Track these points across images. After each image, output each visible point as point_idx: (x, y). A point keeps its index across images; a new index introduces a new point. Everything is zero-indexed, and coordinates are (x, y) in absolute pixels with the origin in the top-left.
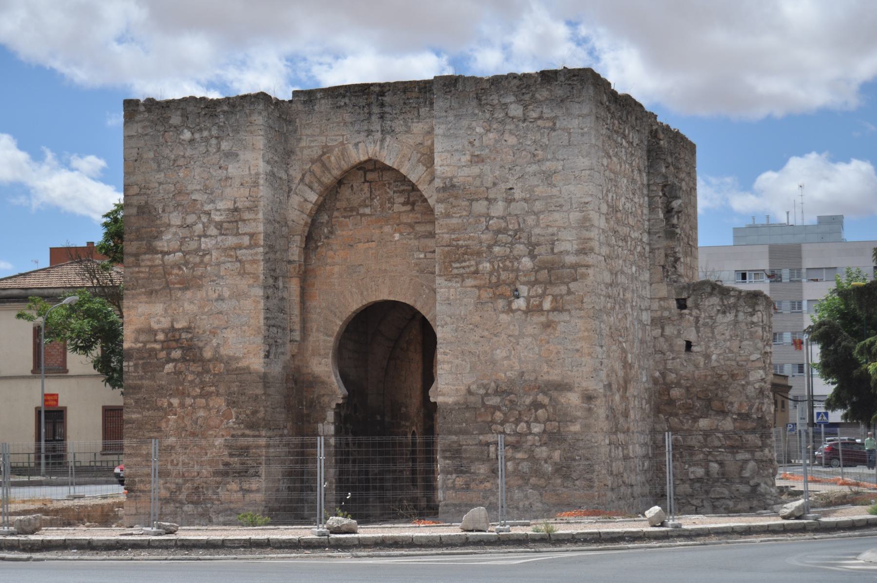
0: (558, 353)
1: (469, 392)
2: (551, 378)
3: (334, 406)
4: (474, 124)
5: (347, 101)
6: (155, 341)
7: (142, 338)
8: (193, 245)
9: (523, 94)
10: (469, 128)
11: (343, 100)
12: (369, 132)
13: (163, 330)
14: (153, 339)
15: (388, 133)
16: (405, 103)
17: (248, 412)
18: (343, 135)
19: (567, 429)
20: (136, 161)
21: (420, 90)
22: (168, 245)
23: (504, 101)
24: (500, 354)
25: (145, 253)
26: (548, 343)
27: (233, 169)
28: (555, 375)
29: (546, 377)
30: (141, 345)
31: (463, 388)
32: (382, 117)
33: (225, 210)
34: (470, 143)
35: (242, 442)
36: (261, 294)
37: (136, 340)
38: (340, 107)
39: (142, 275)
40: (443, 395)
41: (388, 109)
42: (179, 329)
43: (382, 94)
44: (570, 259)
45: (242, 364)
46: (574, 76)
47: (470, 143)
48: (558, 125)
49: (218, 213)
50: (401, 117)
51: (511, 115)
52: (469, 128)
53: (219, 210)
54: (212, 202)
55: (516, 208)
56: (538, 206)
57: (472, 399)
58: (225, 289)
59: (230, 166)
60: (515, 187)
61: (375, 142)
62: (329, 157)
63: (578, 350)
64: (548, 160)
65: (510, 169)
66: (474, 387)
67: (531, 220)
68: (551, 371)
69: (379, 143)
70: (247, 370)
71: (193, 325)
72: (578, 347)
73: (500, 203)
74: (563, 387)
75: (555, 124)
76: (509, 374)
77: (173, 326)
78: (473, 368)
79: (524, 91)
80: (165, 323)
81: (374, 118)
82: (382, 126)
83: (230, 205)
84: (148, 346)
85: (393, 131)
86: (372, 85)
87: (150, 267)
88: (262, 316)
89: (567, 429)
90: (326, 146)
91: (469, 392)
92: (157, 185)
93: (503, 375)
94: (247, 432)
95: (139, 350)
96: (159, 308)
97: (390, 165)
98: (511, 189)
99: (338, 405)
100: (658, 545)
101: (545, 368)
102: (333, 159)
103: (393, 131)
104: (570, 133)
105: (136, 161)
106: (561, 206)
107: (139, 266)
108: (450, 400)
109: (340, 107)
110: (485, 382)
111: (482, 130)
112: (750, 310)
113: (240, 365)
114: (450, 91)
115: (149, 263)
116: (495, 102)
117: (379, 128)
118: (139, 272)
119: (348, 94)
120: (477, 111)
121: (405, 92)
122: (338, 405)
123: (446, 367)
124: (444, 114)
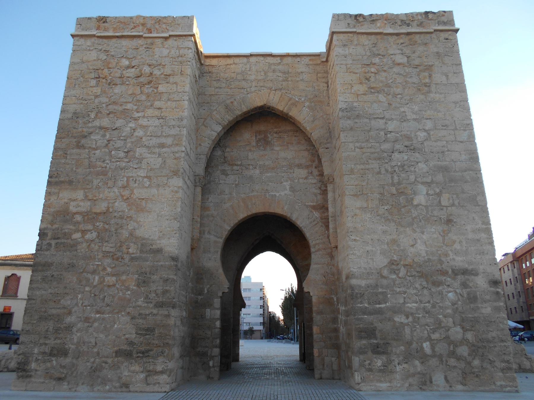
3: (220, 294)
96: (80, 194)
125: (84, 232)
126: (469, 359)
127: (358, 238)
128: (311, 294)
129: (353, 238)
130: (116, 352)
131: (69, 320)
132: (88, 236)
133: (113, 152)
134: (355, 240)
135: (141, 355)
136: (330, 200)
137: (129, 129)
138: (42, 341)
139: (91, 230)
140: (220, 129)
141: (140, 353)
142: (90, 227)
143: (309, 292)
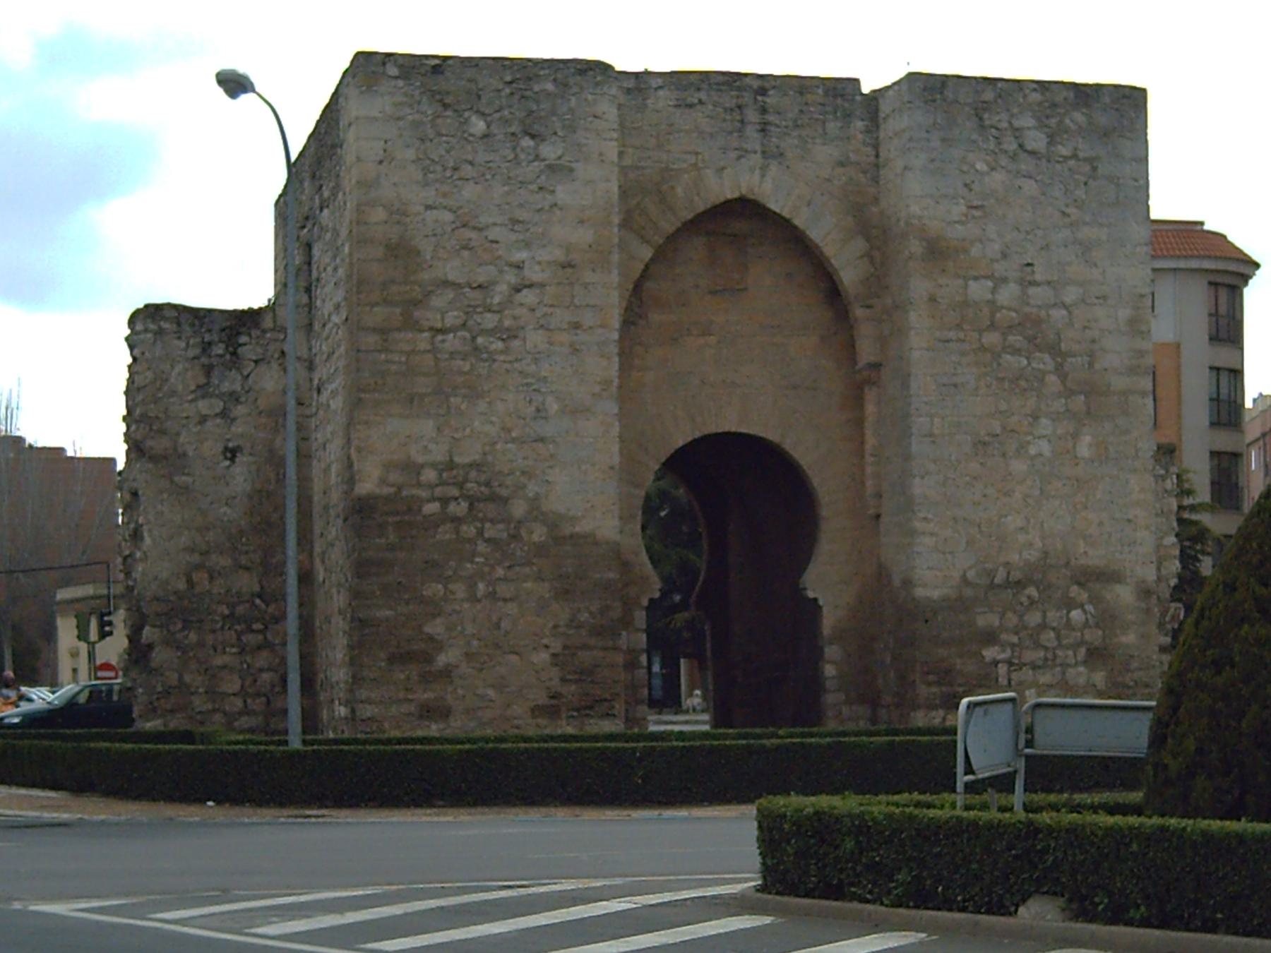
0: (1101, 524)
1: (965, 580)
2: (1090, 563)
3: (645, 603)
4: (971, 156)
5: (703, 95)
6: (419, 485)
7: (394, 477)
8: (490, 320)
9: (1047, 117)
10: (964, 160)
11: (696, 95)
12: (743, 153)
13: (433, 465)
14: (414, 482)
15: (773, 157)
16: (801, 111)
17: (593, 609)
18: (697, 154)
19: (1116, 640)
20: (381, 162)
21: (826, 93)
22: (443, 319)
23: (1016, 123)
24: (1014, 521)
25: (399, 330)
26: (1086, 508)
27: (563, 193)
28: (1095, 558)
29: (1082, 561)
30: (392, 490)
31: (956, 575)
32: (763, 130)
33: (549, 263)
34: (966, 185)
35: (585, 657)
36: (616, 410)
37: (383, 481)
38: (691, 106)
39: (394, 368)
40: (925, 585)
41: (771, 118)
42: (464, 466)
43: (763, 91)
44: (1119, 383)
45: (583, 527)
46: (1124, 97)
47: (966, 185)
48: (1100, 171)
49: (537, 268)
50: (795, 133)
51: (1029, 148)
52: (964, 160)
53: (539, 263)
54: (528, 245)
55: (1039, 294)
56: (1071, 294)
57: (968, 592)
58: (550, 399)
59: (559, 188)
60: (1035, 262)
61: (752, 170)
62: (673, 188)
63: (1129, 521)
64: (1085, 223)
65: (1028, 233)
66: (971, 575)
67: (1058, 314)
68: (1091, 553)
69: (757, 172)
70: (590, 539)
71: (490, 458)
72: (1131, 517)
73: (1012, 285)
74: (1109, 576)
75: (1094, 169)
76: (1025, 555)
77: (451, 461)
78: (970, 543)
79: (1048, 111)
80: (438, 453)
81: (751, 132)
82: (763, 145)
83: (559, 255)
84: (404, 493)
85: (782, 154)
86: (746, 75)
87: (408, 354)
88: (616, 448)
89: (1116, 640)
90: (667, 169)
91: (965, 580)
92: (421, 209)
93: (1017, 557)
94: (592, 641)
95: (388, 499)
96: (427, 427)
97: (778, 211)
98: (1029, 265)
99: (651, 600)
100: (355, 820)
101: (1082, 547)
102: (679, 190)
103: (782, 154)
104: (1118, 185)
105: (381, 162)
106: (1104, 298)
107: (387, 350)
108: (936, 594)
109: (691, 106)
110: (989, 566)
111: (985, 168)
112: (1162, 472)
113: (577, 529)
114: (934, 101)
115: (407, 348)
116: (1004, 125)
117: (758, 148)
118: (387, 361)
119: (705, 86)
120: (975, 136)
121: (801, 93)
122: (651, 600)
123: (928, 541)
124: (926, 135)
125: (445, 501)
126: (1020, 151)
127: (930, 516)
128: (821, 603)
129: (921, 515)
130: (533, 710)
131: (442, 660)
132: (452, 508)
133: (480, 340)
134: (925, 519)
135: (575, 714)
136: (870, 419)
137: (504, 287)
138: (401, 695)
139: (456, 499)
140: (650, 255)
141: (573, 710)
142: (455, 492)
143: (815, 600)
